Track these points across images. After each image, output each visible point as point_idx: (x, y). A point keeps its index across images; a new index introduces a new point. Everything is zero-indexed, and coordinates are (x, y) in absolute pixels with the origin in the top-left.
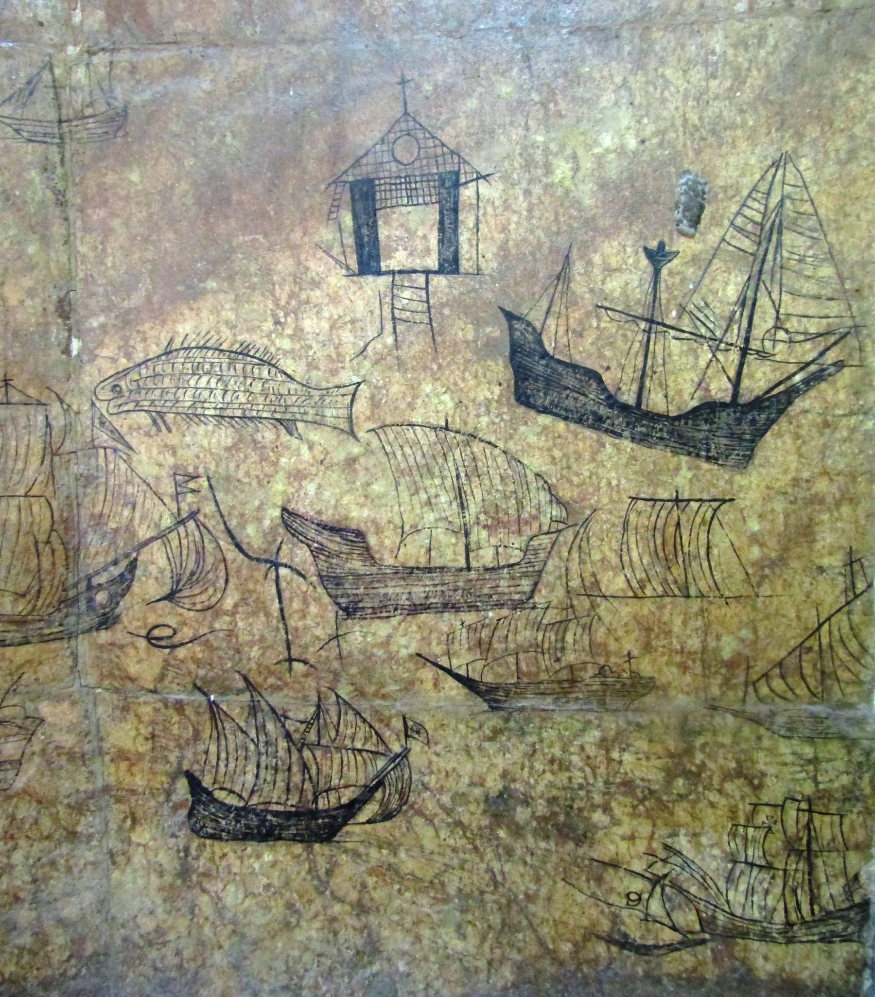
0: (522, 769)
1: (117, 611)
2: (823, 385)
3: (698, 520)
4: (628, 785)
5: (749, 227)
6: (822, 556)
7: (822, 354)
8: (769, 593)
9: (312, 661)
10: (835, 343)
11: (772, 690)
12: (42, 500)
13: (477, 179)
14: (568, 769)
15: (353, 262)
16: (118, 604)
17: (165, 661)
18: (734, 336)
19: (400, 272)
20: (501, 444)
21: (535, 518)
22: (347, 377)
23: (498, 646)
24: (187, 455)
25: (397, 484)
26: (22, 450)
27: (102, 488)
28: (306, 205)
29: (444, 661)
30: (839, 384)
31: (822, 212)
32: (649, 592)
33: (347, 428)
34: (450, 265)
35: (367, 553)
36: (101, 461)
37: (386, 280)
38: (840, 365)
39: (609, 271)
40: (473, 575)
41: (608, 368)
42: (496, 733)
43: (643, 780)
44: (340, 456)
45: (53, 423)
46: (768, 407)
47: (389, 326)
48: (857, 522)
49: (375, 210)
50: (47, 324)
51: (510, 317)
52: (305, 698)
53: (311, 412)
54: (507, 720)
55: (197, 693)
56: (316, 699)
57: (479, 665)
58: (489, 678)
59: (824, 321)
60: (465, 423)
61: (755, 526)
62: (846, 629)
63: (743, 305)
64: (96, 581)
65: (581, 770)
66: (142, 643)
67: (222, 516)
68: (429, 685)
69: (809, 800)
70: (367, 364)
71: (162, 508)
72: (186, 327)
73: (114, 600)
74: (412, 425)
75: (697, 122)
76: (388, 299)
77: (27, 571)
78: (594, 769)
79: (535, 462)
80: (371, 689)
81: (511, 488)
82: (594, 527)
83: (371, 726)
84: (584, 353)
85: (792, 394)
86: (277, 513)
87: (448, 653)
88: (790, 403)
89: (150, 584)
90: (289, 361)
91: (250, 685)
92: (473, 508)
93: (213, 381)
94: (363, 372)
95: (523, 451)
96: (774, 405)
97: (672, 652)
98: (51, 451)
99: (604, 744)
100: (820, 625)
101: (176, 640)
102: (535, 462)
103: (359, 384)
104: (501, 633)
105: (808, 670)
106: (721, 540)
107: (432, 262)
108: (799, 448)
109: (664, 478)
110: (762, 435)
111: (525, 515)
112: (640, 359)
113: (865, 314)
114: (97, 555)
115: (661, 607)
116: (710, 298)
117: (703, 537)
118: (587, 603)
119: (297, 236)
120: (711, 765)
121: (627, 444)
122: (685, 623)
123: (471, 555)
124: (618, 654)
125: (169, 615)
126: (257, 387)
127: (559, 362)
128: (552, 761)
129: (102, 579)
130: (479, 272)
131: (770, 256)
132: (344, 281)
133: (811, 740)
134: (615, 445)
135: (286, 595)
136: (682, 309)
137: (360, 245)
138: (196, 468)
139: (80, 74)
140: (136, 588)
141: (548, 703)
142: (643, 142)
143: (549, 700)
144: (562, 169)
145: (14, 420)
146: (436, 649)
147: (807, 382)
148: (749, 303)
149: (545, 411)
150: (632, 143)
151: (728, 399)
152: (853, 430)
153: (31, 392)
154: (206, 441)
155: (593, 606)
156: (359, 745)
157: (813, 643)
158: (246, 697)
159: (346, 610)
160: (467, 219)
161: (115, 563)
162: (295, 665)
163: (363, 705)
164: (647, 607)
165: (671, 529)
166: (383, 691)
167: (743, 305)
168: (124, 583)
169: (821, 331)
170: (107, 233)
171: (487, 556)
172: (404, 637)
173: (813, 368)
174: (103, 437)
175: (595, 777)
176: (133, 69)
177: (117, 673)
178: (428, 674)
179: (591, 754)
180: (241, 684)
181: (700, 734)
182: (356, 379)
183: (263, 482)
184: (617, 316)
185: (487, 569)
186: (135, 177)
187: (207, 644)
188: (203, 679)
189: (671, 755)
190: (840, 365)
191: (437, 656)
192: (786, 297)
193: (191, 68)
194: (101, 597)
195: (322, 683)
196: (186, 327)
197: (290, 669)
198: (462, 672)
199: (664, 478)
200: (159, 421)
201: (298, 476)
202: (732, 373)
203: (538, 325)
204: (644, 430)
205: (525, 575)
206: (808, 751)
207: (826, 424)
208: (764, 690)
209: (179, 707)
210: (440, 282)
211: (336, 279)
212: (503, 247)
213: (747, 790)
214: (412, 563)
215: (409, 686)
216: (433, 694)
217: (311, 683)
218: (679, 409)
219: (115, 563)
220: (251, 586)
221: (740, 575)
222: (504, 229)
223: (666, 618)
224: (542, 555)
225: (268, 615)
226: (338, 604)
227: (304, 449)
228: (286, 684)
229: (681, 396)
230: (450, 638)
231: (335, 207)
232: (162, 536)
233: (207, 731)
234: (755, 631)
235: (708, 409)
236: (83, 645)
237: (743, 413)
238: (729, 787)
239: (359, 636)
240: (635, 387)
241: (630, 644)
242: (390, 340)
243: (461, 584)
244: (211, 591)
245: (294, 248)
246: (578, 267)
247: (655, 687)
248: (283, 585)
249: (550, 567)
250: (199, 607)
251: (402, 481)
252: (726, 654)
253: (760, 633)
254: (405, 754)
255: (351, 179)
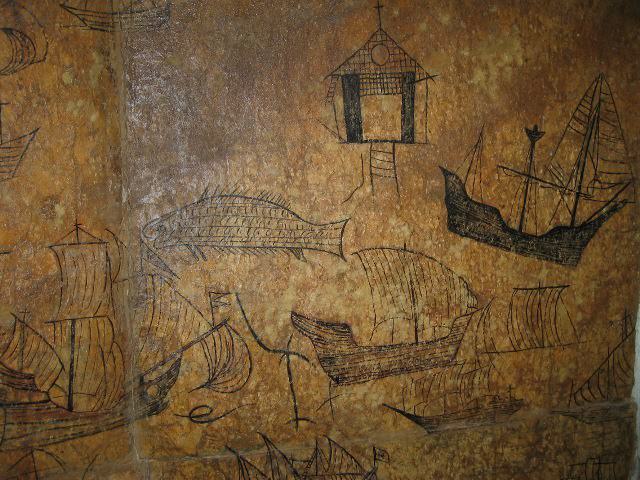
0: (447, 468)
1: (165, 400)
2: (617, 214)
3: (550, 299)
4: (506, 467)
5: (583, 118)
6: (612, 316)
7: (616, 196)
8: (585, 340)
9: (312, 418)
10: (623, 190)
11: (583, 397)
12: (105, 319)
13: (427, 79)
14: (473, 464)
15: (345, 137)
16: (166, 394)
17: (203, 432)
18: (573, 185)
19: (376, 141)
20: (439, 259)
21: (458, 306)
22: (338, 216)
23: (434, 392)
24: (219, 279)
25: (372, 290)
26: (90, 281)
27: (150, 307)
28: (311, 90)
29: (400, 407)
30: (624, 213)
31: (619, 110)
32: (522, 347)
33: (338, 253)
34: (409, 137)
35: (353, 342)
36: (150, 285)
37: (364, 148)
38: (625, 202)
39: (506, 143)
40: (419, 347)
41: (504, 206)
42: (432, 448)
43: (514, 462)
45: (111, 257)
46: (589, 229)
47: (367, 178)
48: (629, 293)
49: (359, 97)
50: (106, 178)
51: (446, 173)
52: (307, 445)
53: (314, 241)
54: (437, 439)
55: (228, 452)
56: (314, 443)
57: (422, 407)
58: (428, 414)
59: (618, 176)
60: (417, 245)
61: (580, 301)
62: (621, 357)
63: (578, 166)
64: (147, 379)
65: (481, 463)
66: (185, 421)
67: (247, 321)
68: (390, 423)
69: (599, 457)
70: (353, 206)
71: (200, 318)
73: (163, 391)
74: (382, 248)
75: (556, 50)
76: (368, 161)
77: (97, 376)
78: (487, 461)
80: (353, 432)
81: (444, 287)
82: (493, 310)
83: (352, 457)
84: (489, 196)
85: (602, 219)
86: (289, 315)
87: (403, 401)
88: (600, 226)
90: (298, 205)
92: (421, 303)
93: (240, 222)
94: (350, 212)
95: (452, 262)
96: (592, 227)
97: (534, 381)
98: (111, 280)
99: (494, 444)
100: (609, 356)
101: (212, 416)
103: (347, 220)
104: (436, 382)
105: (602, 383)
106: (562, 310)
107: (397, 134)
108: (603, 253)
109: (532, 275)
110: (585, 245)
111: (452, 305)
112: (522, 200)
113: (637, 171)
114: (147, 355)
115: (529, 356)
116: (561, 162)
117: (553, 309)
118: (487, 358)
119: (303, 114)
120: (551, 447)
121: (513, 255)
122: (541, 363)
123: (419, 334)
124: (503, 388)
126: (274, 224)
127: (476, 203)
128: (464, 461)
129: (154, 376)
130: (427, 143)
131: (592, 137)
132: (337, 147)
133: (601, 423)
134: (506, 256)
135: (294, 374)
136: (546, 169)
137: (347, 121)
138: (227, 287)
140: (181, 380)
141: (462, 424)
142: (526, 60)
143: (463, 422)
145: (83, 256)
146: (395, 398)
147: (608, 213)
148: (582, 164)
149: (466, 235)
150: (521, 62)
151: (569, 224)
152: (629, 240)
153: (95, 233)
155: (491, 359)
156: (343, 471)
157: (605, 367)
158: (264, 450)
159: (337, 380)
160: (420, 106)
161: (163, 363)
162: (300, 423)
163: (347, 444)
164: (522, 355)
165: (536, 307)
166: (361, 432)
167: (578, 166)
169: (617, 181)
171: (428, 334)
172: (372, 393)
173: (612, 204)
175: (488, 464)
177: (166, 446)
178: (389, 417)
179: (486, 452)
180: (261, 441)
181: (546, 429)
182: (344, 217)
184: (509, 172)
185: (428, 343)
187: (237, 416)
188: (232, 441)
189: (530, 444)
190: (625, 202)
191: (395, 404)
192: (600, 162)
195: (319, 432)
197: (297, 427)
198: (411, 412)
199: (532, 275)
200: (197, 253)
202: (571, 207)
203: (463, 178)
204: (523, 245)
205: (451, 343)
206: (600, 429)
207: (617, 237)
208: (579, 398)
209: (215, 464)
210: (401, 148)
211: (332, 146)
212: (442, 125)
213: (568, 458)
214: (381, 343)
216: (392, 429)
217: (312, 434)
218: (542, 231)
219: (163, 363)
220: (269, 370)
221: (571, 331)
222: (443, 114)
223: (531, 361)
224: (462, 330)
225: (282, 390)
226: (331, 377)
227: (309, 270)
228: (294, 436)
229: (543, 224)
230: (404, 390)
231: (330, 95)
232: (201, 340)
234: (577, 363)
235: (558, 230)
237: (577, 232)
238: (560, 458)
239: (350, 395)
240: (518, 219)
241: (510, 381)
242: (369, 190)
243: (412, 354)
244: (239, 376)
246: (488, 140)
247: (523, 405)
248: (293, 367)
249: (466, 338)
250: (230, 389)
251: (376, 288)
252: (562, 380)
253: (580, 365)
254: (374, 472)
255: (342, 73)
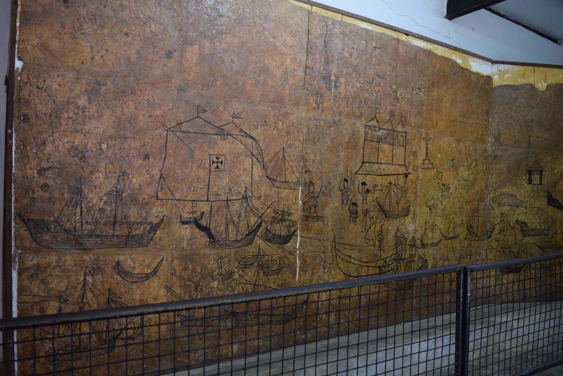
24: (503, 211)
34: (541, 184)
35: (527, 227)
44: (524, 212)
72: (504, 190)
73: (491, 233)
79: (550, 214)
84: (557, 198)
89: (496, 231)
91: (509, 248)
98: (484, 209)
102: (550, 214)
107: (539, 183)
119: (521, 178)
125: (499, 236)
139: (490, 149)
141: (549, 250)
144: (556, 171)
154: (506, 209)
160: (543, 177)
168: (493, 231)
170: (493, 174)
171: (543, 228)
174: (490, 207)
176: (498, 149)
178: (534, 245)
183: (514, 215)
186: (498, 166)
193: (506, 150)
194: (489, 233)
196: (504, 190)
201: (519, 214)
210: (539, 186)
211: (526, 185)
215: (531, 247)
232: (499, 223)
233: (503, 255)
236: (485, 241)
239: (526, 239)
241: (560, 241)
245: (520, 180)
